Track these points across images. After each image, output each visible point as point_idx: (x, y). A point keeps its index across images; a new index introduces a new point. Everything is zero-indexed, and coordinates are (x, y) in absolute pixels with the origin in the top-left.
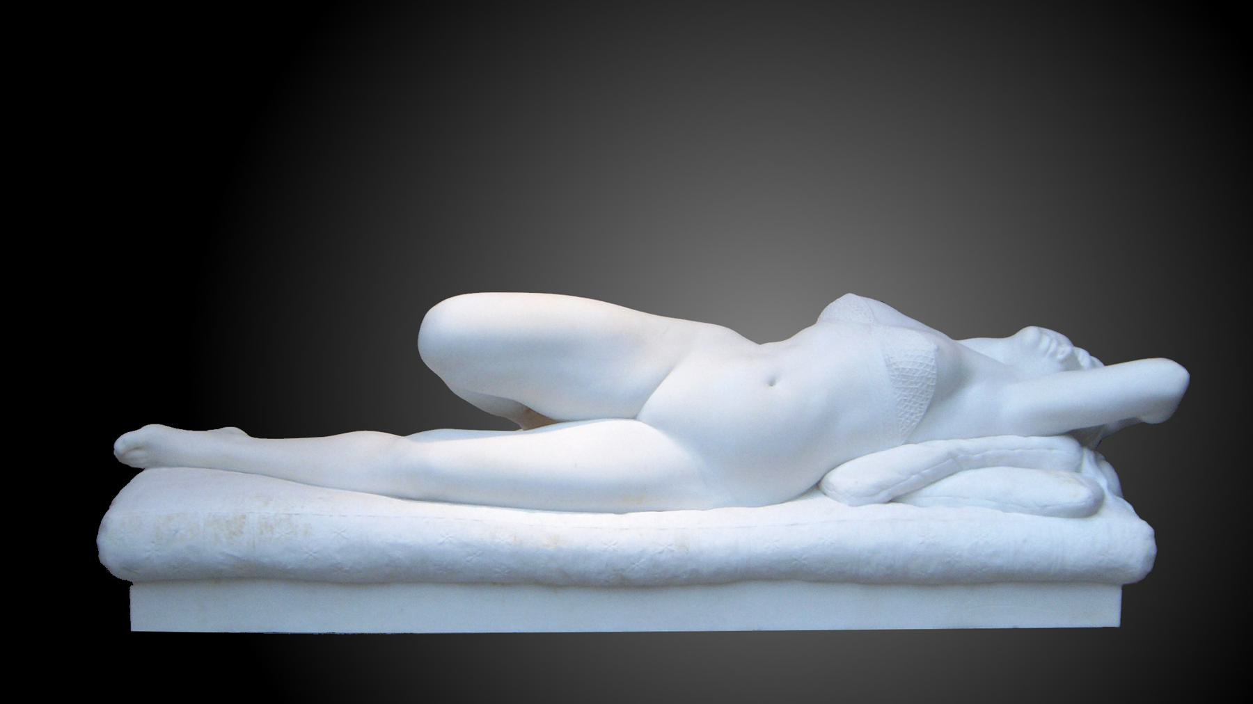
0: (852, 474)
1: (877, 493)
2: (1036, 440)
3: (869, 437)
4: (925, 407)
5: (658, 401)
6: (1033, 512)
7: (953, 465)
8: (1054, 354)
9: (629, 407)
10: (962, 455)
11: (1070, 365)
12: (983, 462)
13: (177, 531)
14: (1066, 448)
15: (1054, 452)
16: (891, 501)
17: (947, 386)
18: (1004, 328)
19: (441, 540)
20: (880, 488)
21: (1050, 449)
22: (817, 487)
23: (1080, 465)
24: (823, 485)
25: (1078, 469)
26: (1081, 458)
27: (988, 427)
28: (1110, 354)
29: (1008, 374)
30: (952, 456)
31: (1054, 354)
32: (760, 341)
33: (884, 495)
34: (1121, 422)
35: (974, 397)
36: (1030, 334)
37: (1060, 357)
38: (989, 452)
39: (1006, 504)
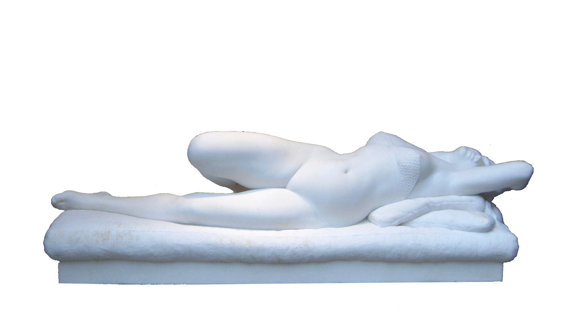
0: (382, 213)
2: (465, 198)
3: (390, 196)
5: (295, 180)
6: (463, 230)
7: (427, 209)
8: (473, 159)
9: (282, 183)
10: (431, 204)
12: (441, 207)
15: (473, 203)
16: (400, 225)
19: (198, 242)
21: (471, 201)
23: (484, 209)
26: (485, 206)
27: (443, 192)
30: (427, 205)
31: (473, 159)
33: (396, 222)
35: (437, 178)
37: (475, 160)
39: (451, 226)
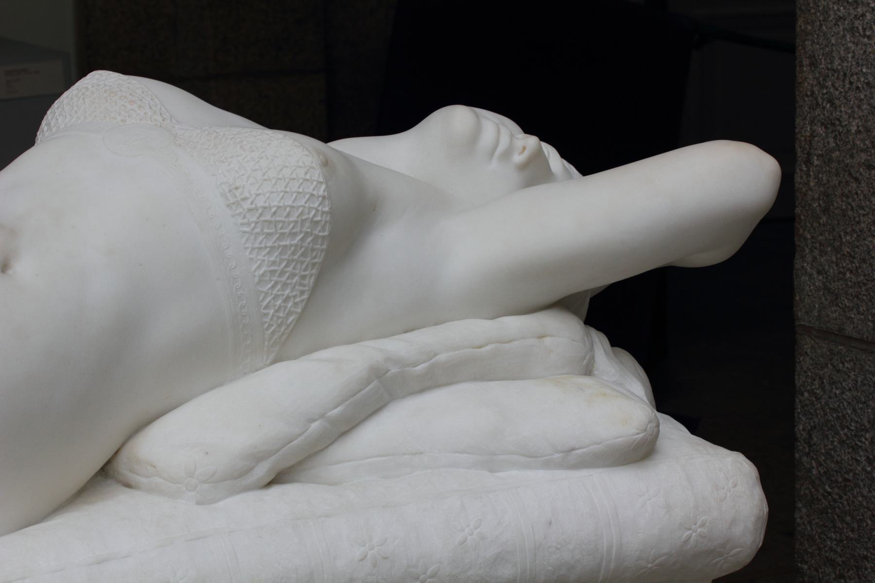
1: (248, 471)
4: (310, 282)
6: (548, 465)
7: (380, 391)
8: (507, 154)
10: (394, 370)
11: (534, 174)
13: (464, 542)
14: (565, 333)
15: (548, 340)
16: (278, 479)
17: (345, 229)
18: (396, 116)
20: (257, 457)
21: (541, 337)
22: (107, 474)
24: (122, 466)
25: (588, 371)
28: (592, 154)
29: (432, 201)
30: (377, 374)
31: (507, 154)
32: (28, 142)
33: (262, 471)
34: (221, 385)
35: (388, 248)
36: (455, 121)
37: (518, 158)
38: (442, 357)
39: (490, 458)
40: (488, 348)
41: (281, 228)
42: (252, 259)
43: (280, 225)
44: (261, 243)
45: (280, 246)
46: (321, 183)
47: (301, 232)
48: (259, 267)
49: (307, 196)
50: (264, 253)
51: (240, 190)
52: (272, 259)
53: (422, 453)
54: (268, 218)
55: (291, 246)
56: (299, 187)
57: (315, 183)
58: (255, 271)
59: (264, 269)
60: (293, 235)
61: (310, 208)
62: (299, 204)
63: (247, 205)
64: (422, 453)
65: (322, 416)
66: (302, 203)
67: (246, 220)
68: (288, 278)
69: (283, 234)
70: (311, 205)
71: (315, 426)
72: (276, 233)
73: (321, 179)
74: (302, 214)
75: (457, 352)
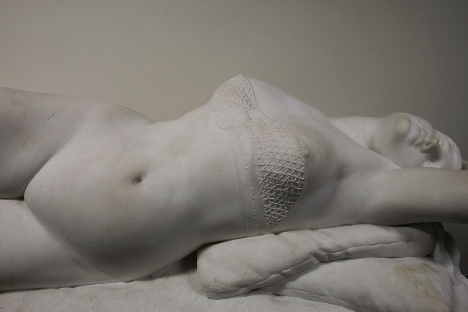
25: (430, 256)
40: (377, 246)
41: (278, 183)
42: (262, 193)
43: (277, 182)
44: (267, 187)
45: (276, 191)
46: (303, 166)
47: (288, 187)
48: (266, 197)
49: (293, 171)
50: (268, 191)
51: (261, 160)
52: (272, 195)
53: (325, 296)
54: (272, 177)
55: (283, 191)
56: (290, 166)
57: (299, 165)
58: (263, 198)
59: (267, 198)
60: (283, 187)
61: (294, 178)
62: (288, 174)
63: (263, 169)
64: (325, 296)
65: (278, 272)
66: (290, 174)
67: (262, 175)
68: (280, 203)
69: (279, 186)
70: (295, 176)
71: (273, 276)
72: (275, 184)
73: (303, 164)
74: (290, 179)
75: (358, 248)
